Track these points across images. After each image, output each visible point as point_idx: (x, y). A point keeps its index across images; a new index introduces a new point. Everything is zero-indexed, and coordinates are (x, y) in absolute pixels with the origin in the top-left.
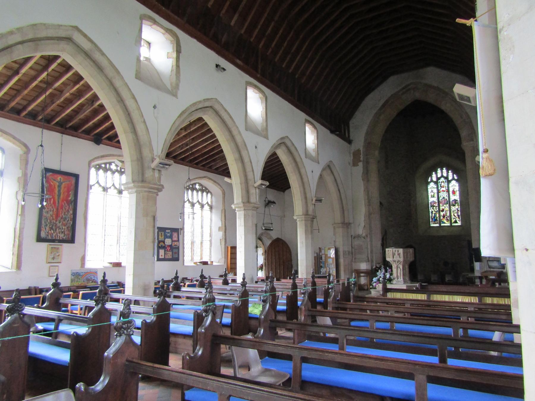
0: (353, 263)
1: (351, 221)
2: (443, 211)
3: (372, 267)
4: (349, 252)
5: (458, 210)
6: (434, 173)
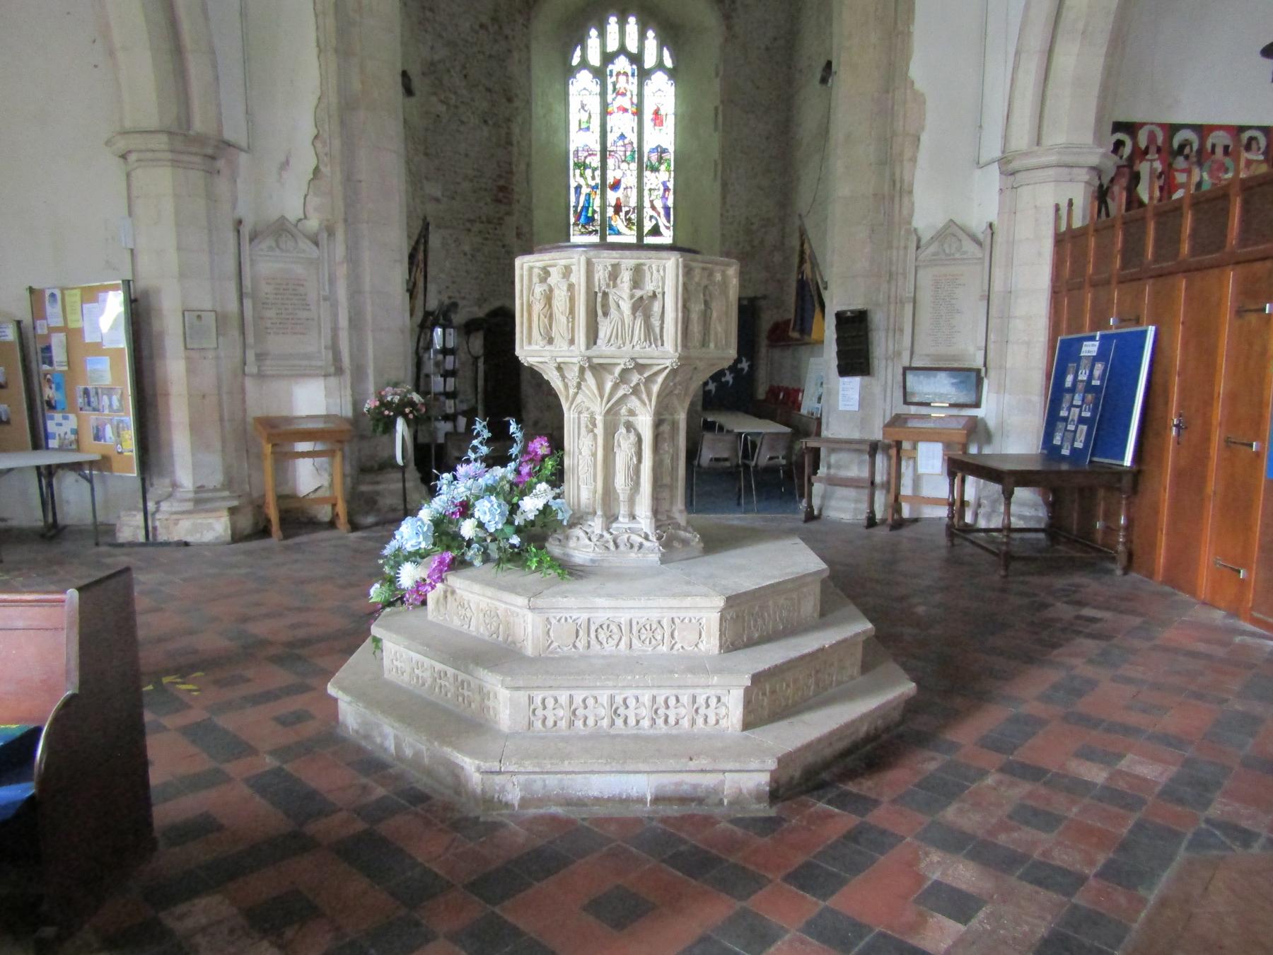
0: (249, 384)
1: (234, 131)
2: (616, 186)
3: (357, 405)
4: (221, 320)
5: (666, 189)
6: (594, 33)
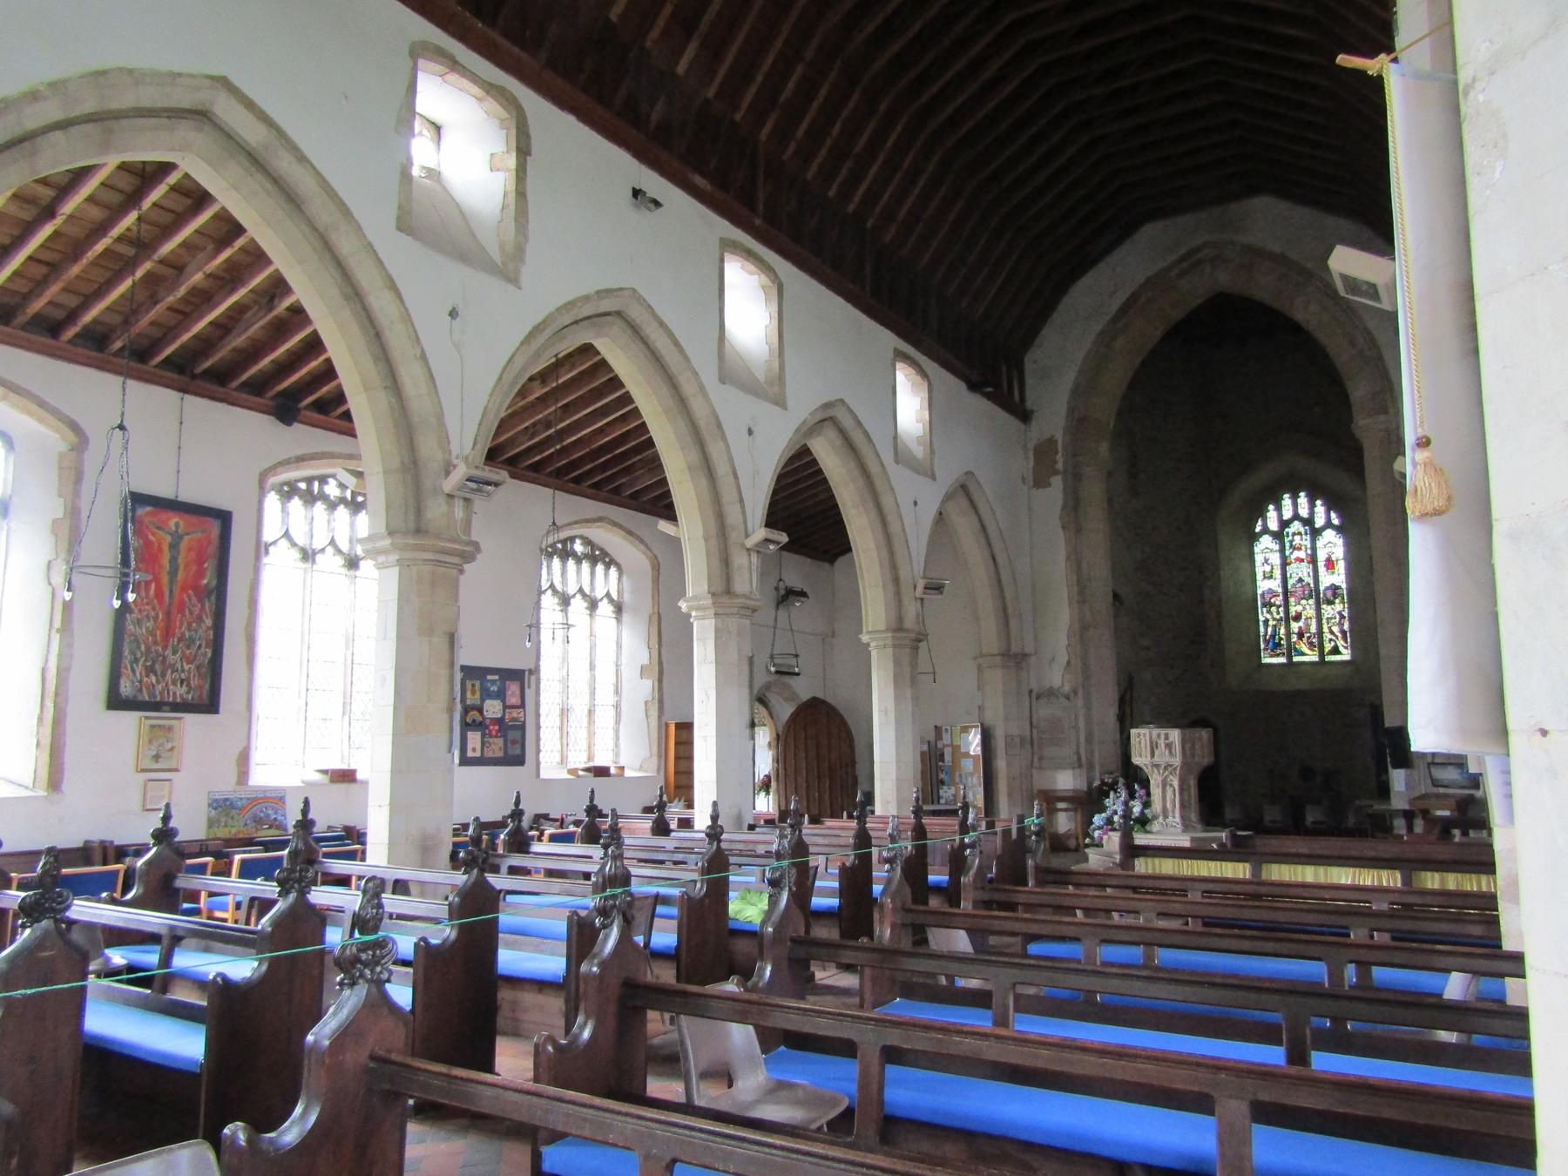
0: (1035, 772)
1: (1029, 649)
2: (1298, 617)
3: (1090, 784)
4: (1022, 739)
5: (1342, 617)
6: (1271, 507)
